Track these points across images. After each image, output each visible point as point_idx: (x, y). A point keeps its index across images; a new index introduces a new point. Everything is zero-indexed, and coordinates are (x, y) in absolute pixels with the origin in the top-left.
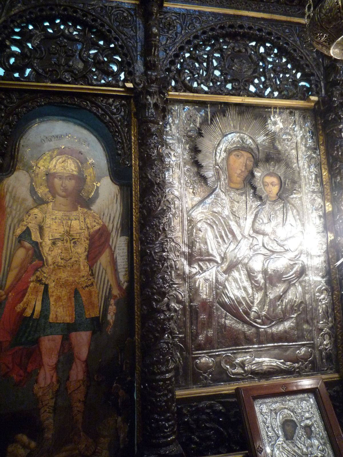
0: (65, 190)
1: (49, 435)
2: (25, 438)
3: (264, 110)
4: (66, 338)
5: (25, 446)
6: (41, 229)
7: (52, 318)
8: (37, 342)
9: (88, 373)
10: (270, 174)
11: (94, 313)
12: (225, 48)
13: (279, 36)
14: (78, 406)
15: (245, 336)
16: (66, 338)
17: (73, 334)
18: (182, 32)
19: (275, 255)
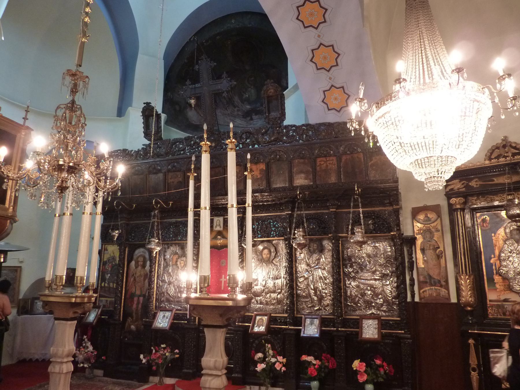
0: (141, 264)
1: (134, 318)
2: (130, 318)
3: (87, 262)
4: (138, 298)
5: (130, 320)
6: (136, 274)
7: (136, 294)
8: (133, 298)
9: (142, 307)
10: (182, 261)
11: (144, 293)
12: (370, 221)
13: (119, 181)
14: (140, 314)
15: (188, 292)
16: (138, 298)
17: (140, 297)
18: (483, 225)
19: (362, 100)
